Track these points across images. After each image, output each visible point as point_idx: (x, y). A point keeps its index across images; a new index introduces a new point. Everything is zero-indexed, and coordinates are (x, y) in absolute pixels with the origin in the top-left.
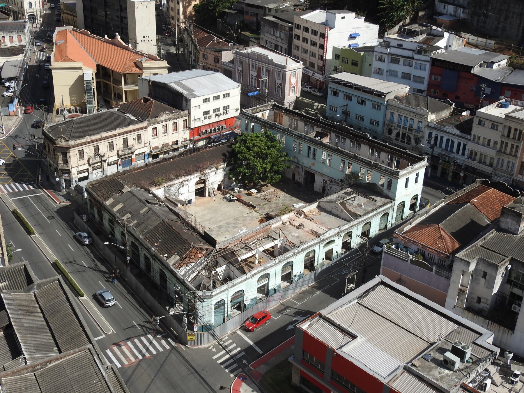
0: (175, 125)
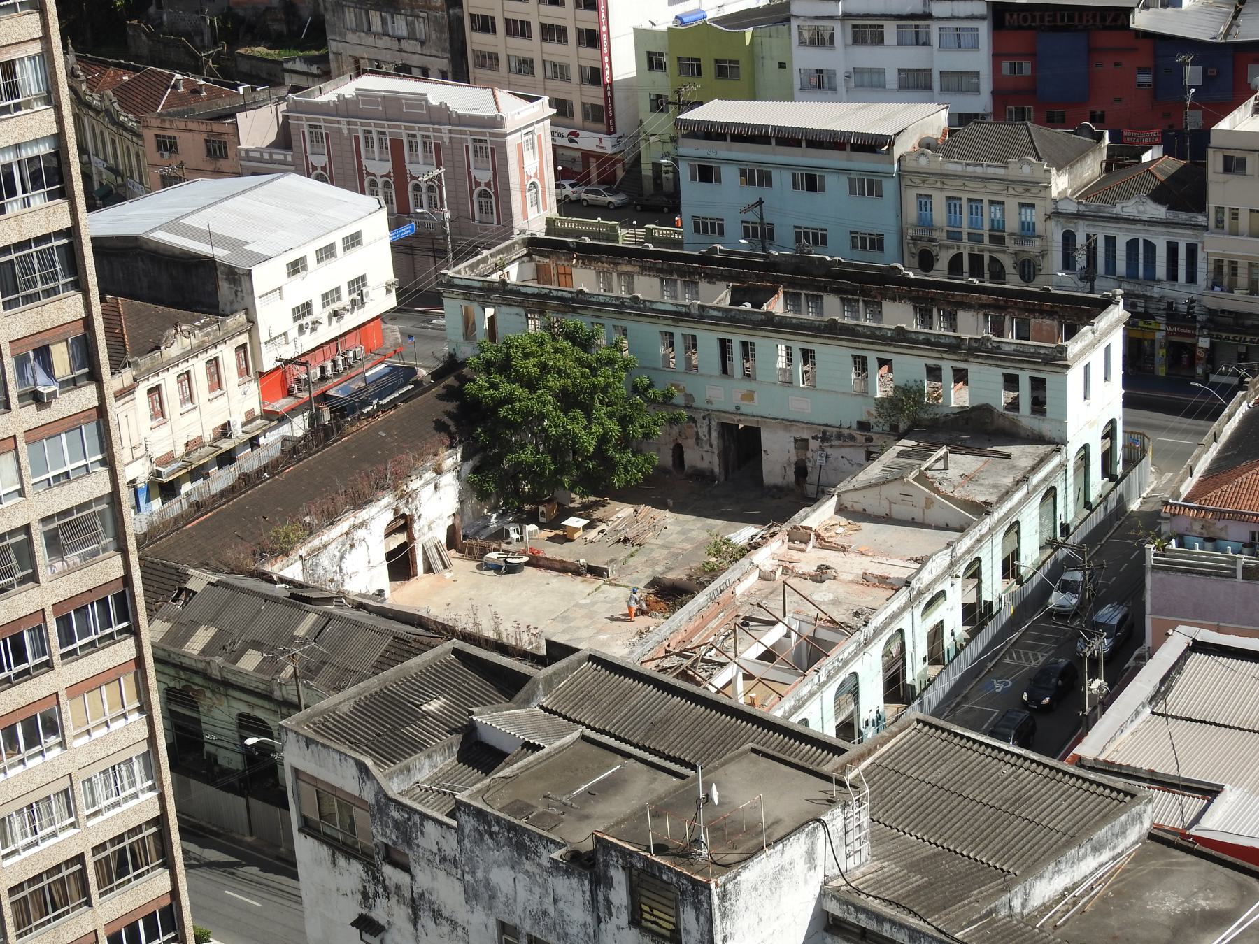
0: (213, 369)
